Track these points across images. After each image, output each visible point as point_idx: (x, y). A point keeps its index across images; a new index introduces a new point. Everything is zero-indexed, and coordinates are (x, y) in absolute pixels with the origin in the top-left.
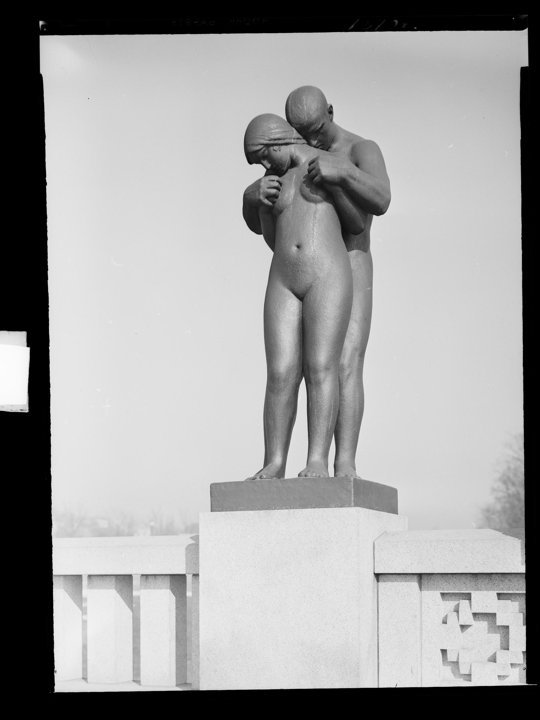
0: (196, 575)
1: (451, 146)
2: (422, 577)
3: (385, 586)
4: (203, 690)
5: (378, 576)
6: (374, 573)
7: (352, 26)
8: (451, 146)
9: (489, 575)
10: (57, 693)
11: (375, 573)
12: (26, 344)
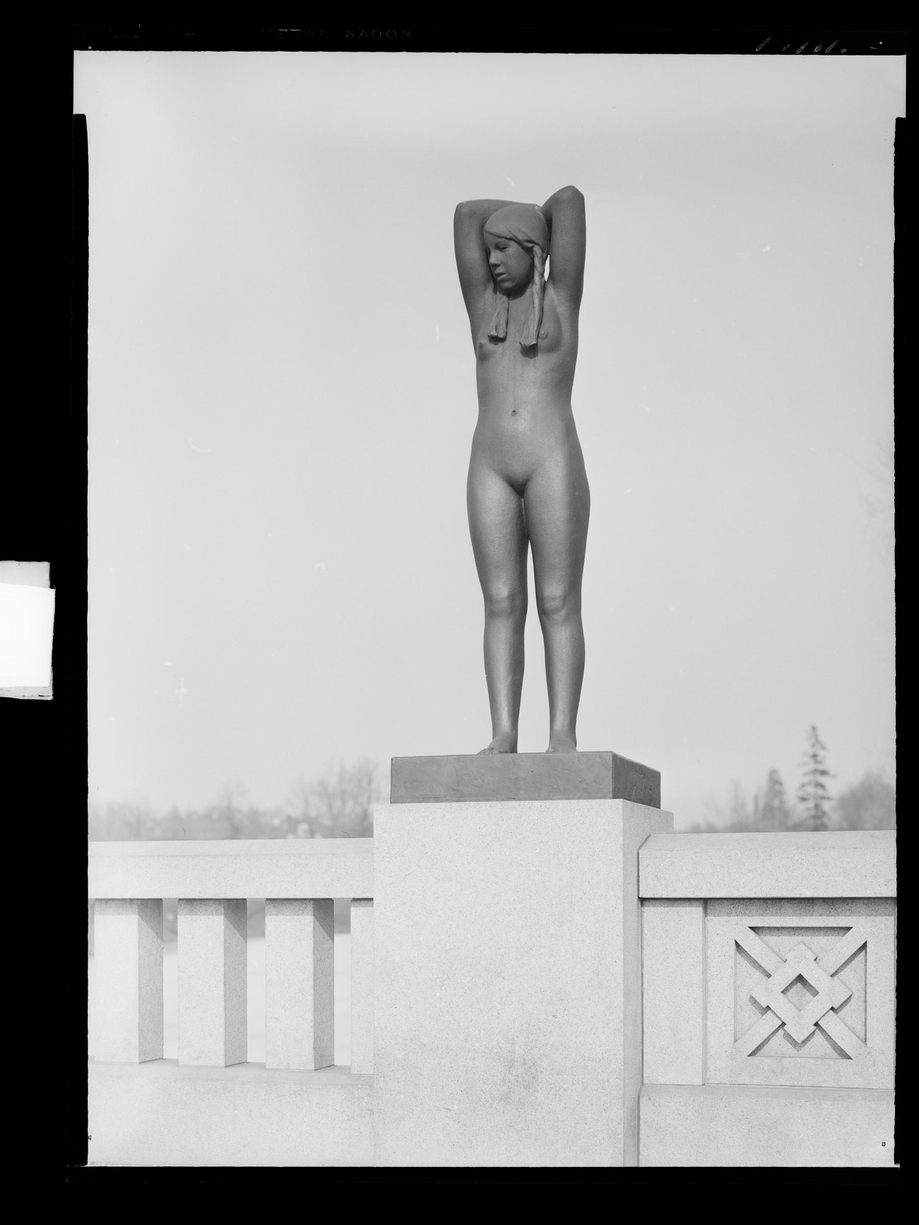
1: (768, 249)
5: (643, 901)
6: (639, 897)
7: (802, 48)
8: (768, 249)
10: (76, 114)
11: (640, 896)
12: (48, 583)
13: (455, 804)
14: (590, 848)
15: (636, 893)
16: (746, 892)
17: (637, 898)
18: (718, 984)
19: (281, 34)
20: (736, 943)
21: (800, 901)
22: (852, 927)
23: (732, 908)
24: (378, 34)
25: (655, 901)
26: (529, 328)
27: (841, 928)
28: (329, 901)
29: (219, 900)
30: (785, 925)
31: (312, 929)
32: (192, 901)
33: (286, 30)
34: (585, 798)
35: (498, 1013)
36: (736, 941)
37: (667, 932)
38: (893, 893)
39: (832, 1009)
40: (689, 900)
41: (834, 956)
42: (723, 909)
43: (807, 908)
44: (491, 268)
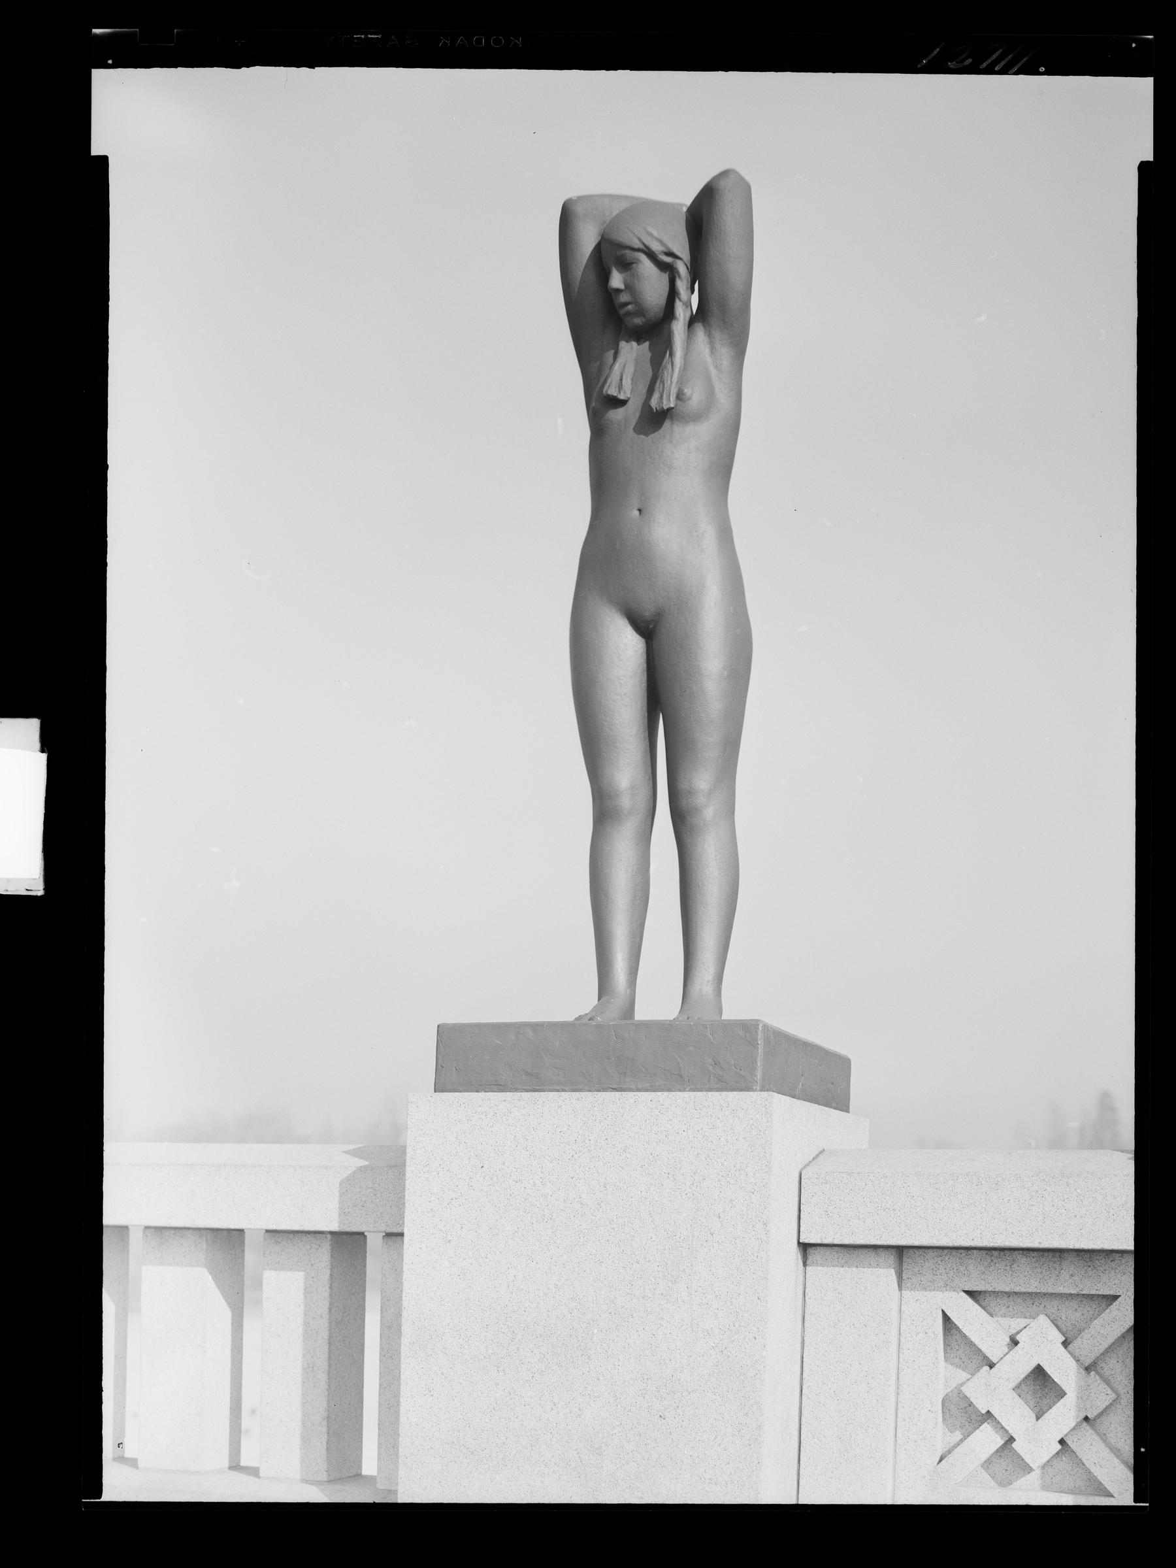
0: (395, 1236)
1: (983, 318)
2: (810, 1259)
3: (822, 1273)
4: (458, 1502)
5: (805, 1248)
6: (799, 1243)
9: (175, 1228)
11: (801, 1241)
12: (38, 745)
13: (526, 1095)
14: (723, 1165)
15: (795, 1236)
16: (959, 1237)
17: (796, 1243)
18: (914, 1375)
19: (356, 41)
20: (946, 1318)
21: (1042, 1253)
22: (1120, 1296)
23: (939, 1262)
24: (479, 41)
25: (825, 1248)
26: (664, 384)
27: (1104, 1297)
28: (359, 1236)
29: (200, 1229)
30: (1017, 1289)
31: (327, 1276)
32: (162, 1230)
33: (363, 36)
34: (719, 1090)
35: (580, 1409)
36: (943, 1311)
37: (841, 1296)
38: (1132, 1248)
39: (1086, 1419)
40: (875, 1247)
41: (1091, 1339)
42: (927, 1263)
43: (1051, 1264)
44: (609, 295)
